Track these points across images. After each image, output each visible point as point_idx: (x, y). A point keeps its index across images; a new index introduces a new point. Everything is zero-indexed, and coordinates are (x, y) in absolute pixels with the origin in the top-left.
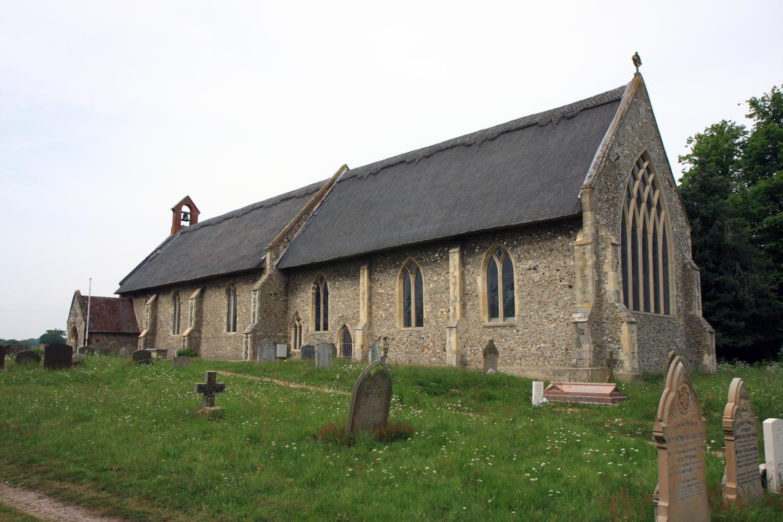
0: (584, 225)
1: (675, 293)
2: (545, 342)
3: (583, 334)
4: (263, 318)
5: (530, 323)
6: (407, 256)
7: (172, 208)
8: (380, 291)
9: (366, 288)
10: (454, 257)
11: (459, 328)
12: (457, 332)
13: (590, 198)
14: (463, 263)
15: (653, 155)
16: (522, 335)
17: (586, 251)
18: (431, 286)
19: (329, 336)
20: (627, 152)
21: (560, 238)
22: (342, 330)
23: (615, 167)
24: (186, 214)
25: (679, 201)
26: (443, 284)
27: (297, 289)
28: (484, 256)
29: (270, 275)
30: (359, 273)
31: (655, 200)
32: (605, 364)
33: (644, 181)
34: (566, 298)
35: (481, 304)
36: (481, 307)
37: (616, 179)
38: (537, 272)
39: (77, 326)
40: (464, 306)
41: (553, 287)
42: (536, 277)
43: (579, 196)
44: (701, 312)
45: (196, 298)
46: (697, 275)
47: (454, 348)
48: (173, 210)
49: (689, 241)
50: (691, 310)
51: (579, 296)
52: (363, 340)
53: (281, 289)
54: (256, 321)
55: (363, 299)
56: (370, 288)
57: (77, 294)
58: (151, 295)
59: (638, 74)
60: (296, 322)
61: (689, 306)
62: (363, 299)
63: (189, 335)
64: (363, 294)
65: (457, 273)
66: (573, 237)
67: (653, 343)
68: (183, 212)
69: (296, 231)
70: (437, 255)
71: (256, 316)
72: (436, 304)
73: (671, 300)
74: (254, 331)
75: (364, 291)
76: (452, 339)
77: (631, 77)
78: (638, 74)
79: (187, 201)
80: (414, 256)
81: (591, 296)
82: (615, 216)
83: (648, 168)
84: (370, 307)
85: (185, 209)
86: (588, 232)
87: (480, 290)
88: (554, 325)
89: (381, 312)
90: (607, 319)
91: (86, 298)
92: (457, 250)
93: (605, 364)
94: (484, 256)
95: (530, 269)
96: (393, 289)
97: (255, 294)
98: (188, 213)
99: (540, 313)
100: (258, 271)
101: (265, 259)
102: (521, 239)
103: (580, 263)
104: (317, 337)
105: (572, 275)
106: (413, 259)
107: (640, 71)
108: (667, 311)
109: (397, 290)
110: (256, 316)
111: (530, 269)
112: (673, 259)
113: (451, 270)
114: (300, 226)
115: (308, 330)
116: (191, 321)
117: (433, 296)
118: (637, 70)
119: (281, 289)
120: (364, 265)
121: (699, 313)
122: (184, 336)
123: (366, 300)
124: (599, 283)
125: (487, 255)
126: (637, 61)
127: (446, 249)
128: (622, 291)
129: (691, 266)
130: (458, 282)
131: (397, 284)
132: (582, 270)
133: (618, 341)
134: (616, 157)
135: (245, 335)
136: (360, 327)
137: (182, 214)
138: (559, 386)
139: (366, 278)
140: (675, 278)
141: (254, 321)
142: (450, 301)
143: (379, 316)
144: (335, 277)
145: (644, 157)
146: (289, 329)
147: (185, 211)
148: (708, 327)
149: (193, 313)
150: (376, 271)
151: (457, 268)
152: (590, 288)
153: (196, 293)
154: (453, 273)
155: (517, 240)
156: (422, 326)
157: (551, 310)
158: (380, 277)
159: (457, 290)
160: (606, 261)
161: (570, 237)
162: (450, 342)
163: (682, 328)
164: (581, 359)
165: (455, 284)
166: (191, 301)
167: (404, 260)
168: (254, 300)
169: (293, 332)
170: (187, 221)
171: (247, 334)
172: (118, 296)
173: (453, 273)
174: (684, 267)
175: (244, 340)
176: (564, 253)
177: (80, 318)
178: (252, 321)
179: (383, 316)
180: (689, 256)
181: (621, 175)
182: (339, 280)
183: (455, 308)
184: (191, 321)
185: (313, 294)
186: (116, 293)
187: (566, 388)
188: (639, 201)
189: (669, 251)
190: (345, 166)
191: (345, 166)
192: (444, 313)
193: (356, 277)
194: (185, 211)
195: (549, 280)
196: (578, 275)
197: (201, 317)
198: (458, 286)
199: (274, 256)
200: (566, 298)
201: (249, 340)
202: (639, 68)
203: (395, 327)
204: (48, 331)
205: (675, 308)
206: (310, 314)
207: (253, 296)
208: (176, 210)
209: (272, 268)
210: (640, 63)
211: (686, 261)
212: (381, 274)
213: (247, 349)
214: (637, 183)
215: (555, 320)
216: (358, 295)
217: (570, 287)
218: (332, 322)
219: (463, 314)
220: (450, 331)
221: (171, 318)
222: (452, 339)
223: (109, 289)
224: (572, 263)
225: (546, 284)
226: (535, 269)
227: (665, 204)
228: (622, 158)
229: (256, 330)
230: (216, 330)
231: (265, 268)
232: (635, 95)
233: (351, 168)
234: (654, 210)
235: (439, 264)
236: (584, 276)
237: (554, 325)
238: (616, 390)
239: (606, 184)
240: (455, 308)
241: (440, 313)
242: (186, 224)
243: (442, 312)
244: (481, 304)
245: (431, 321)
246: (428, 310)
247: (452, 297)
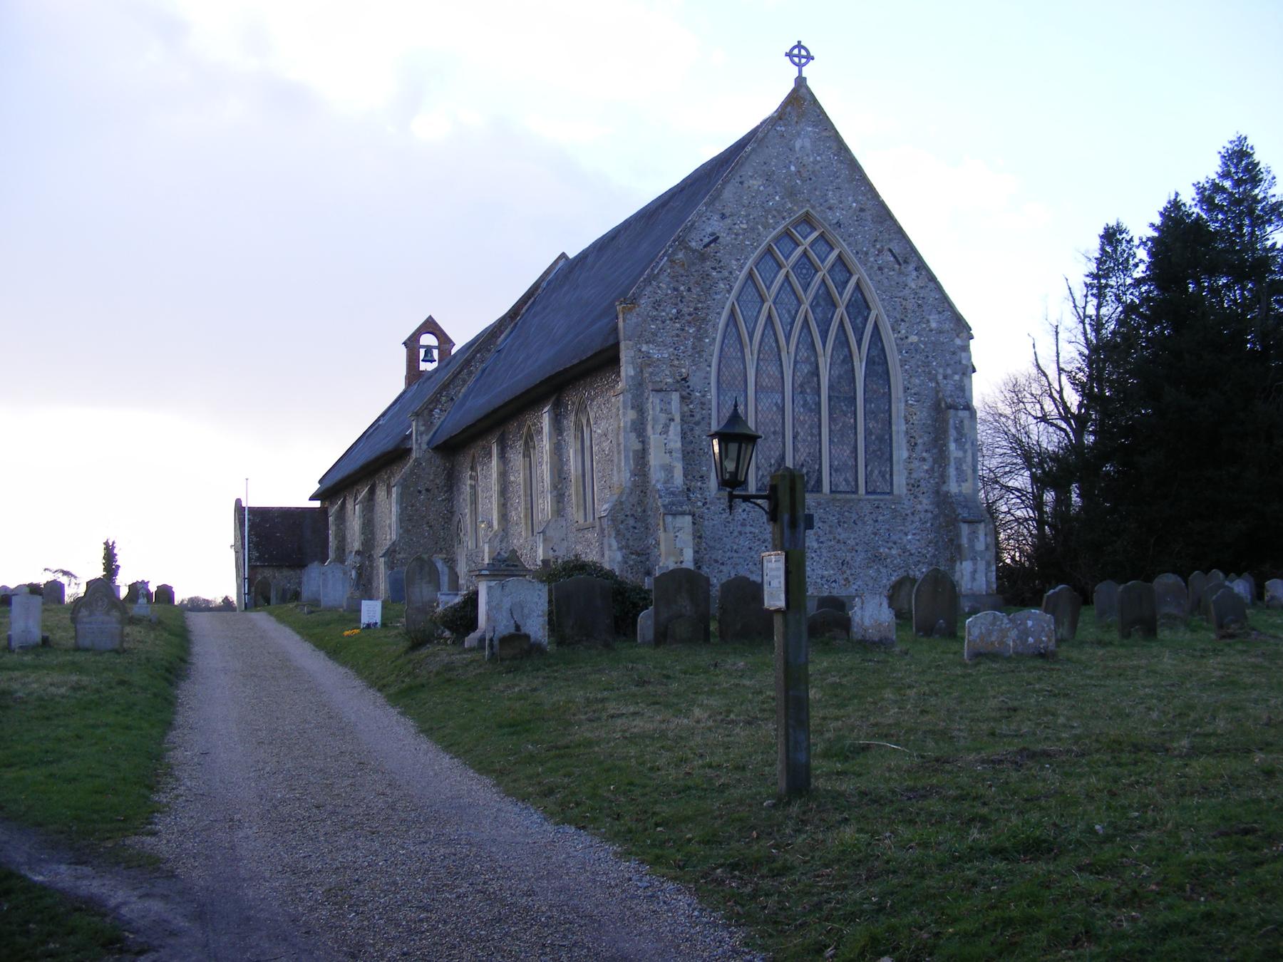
4: (407, 531)
11: (550, 533)
20: (744, 226)
24: (429, 350)
59: (801, 81)
68: (423, 347)
69: (464, 381)
78: (801, 81)
85: (428, 340)
98: (435, 347)
114: (470, 373)
126: (800, 55)
137: (422, 352)
172: (317, 504)
186: (312, 499)
190: (563, 255)
191: (563, 255)
197: (372, 533)
199: (422, 428)
202: (806, 72)
204: (118, 567)
208: (412, 344)
233: (571, 255)
239: (676, 289)
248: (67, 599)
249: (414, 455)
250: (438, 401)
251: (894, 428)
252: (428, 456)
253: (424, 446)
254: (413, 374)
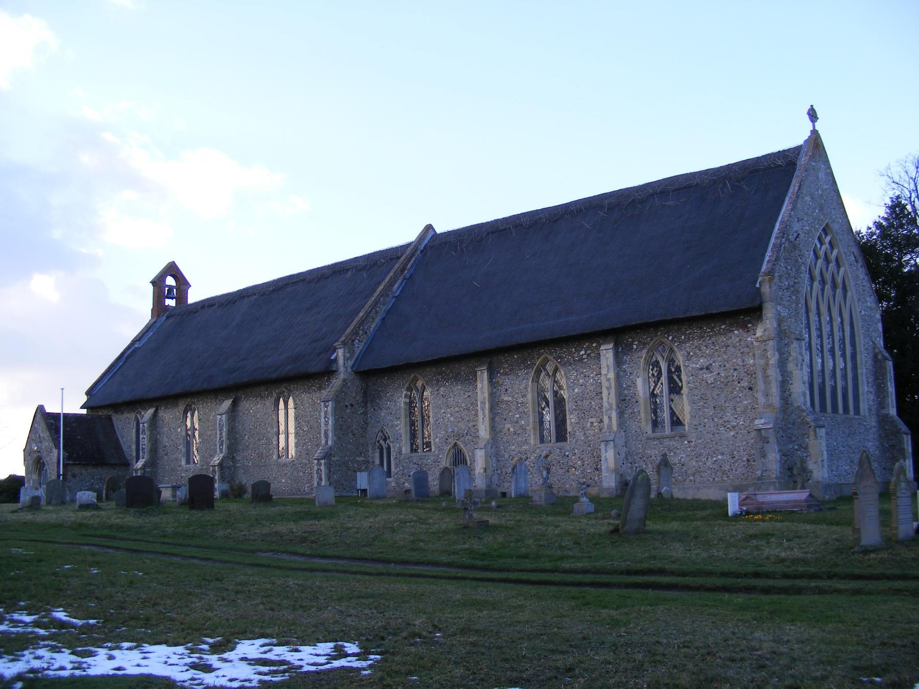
0: (764, 318)
1: (866, 389)
2: (723, 454)
3: (768, 442)
4: (339, 438)
5: (704, 432)
6: (542, 354)
7: (151, 280)
8: (506, 399)
9: (486, 395)
10: (607, 352)
11: (617, 441)
12: (615, 447)
13: (770, 287)
14: (618, 362)
15: (835, 227)
16: (696, 446)
17: (768, 348)
18: (576, 390)
19: (432, 458)
21: (736, 332)
22: (453, 450)
23: (795, 247)
24: (171, 288)
25: (866, 278)
26: (592, 388)
27: (380, 398)
28: (644, 353)
29: (344, 380)
30: (476, 376)
31: (839, 280)
32: (794, 473)
33: (827, 260)
34: (745, 402)
35: (642, 411)
36: (642, 415)
37: (797, 261)
38: (711, 372)
39: (44, 454)
40: (621, 414)
41: (730, 389)
42: (709, 377)
43: (758, 285)
44: (895, 410)
45: (226, 413)
46: (890, 364)
47: (612, 464)
48: (153, 283)
49: (880, 325)
50: (883, 408)
51: (761, 399)
52: (487, 462)
53: (358, 398)
54: (330, 443)
55: (483, 409)
56: (492, 395)
57: (40, 409)
58: (146, 409)
59: (814, 132)
60: (382, 442)
61: (882, 404)
62: (483, 409)
63: (221, 465)
64: (483, 403)
65: (611, 375)
66: (752, 332)
67: (842, 448)
69: (373, 319)
70: (582, 352)
71: (330, 435)
72: (584, 414)
73: (861, 398)
74: (327, 456)
75: (484, 398)
76: (609, 456)
77: (806, 135)
78: (814, 132)
79: (172, 269)
80: (551, 354)
81: (776, 400)
82: (797, 304)
83: (830, 243)
84: (492, 420)
85: (170, 281)
86: (769, 326)
87: (641, 394)
88: (732, 433)
89: (508, 426)
90: (793, 424)
91: (56, 416)
92: (611, 346)
93: (794, 473)
94: (644, 353)
95: (701, 369)
96: (524, 396)
97: (327, 407)
99: (716, 420)
100: (328, 372)
101: (336, 358)
102: (690, 333)
103: (762, 362)
104: (415, 461)
105: (751, 374)
106: (550, 357)
107: (817, 128)
108: (857, 410)
109: (529, 396)
110: (330, 435)
111: (701, 369)
112: (862, 349)
113: (604, 371)
114: (377, 312)
115: (400, 452)
116: (221, 445)
117: (579, 403)
118: (814, 126)
119: (358, 398)
120: (482, 364)
121: (893, 411)
122: (214, 466)
123: (487, 411)
124: (784, 384)
125: (648, 352)
126: (813, 115)
127: (594, 345)
128: (808, 392)
129: (883, 355)
130: (613, 386)
131: (529, 389)
132: (764, 370)
133: (806, 448)
134: (795, 235)
135: (316, 462)
136: (482, 445)
138: (753, 497)
139: (486, 382)
140: (864, 371)
141: (327, 442)
142: (604, 410)
143: (506, 430)
144: (438, 381)
145: (825, 231)
146: (370, 452)
147: (169, 283)
148: (903, 427)
149: (224, 434)
150: (498, 372)
151: (612, 370)
152: (775, 390)
153: (227, 404)
154: (606, 375)
155: (685, 334)
156: (565, 440)
157: (729, 416)
158: (506, 381)
159: (613, 395)
160: (790, 359)
161: (748, 331)
162: (606, 459)
163: (874, 430)
164: (766, 471)
165: (608, 388)
166: (219, 417)
167: (538, 358)
168: (326, 413)
169: (377, 455)
170: (172, 298)
171: (318, 460)
172: (84, 411)
173: (606, 375)
174: (875, 356)
175: (316, 468)
176: (742, 350)
177: (48, 443)
178: (323, 442)
179: (511, 430)
180: (880, 342)
181: (801, 256)
182: (444, 385)
183: (610, 418)
184: (221, 445)
185: (405, 403)
187: (760, 498)
188: (823, 282)
189: (857, 339)
191: (429, 228)
192: (595, 424)
193: (471, 379)
194: (169, 283)
195: (726, 381)
196: (760, 375)
198: (613, 391)
199: (348, 355)
200: (745, 402)
201: (323, 468)
203: (528, 444)
205: (866, 407)
206: (402, 431)
207: (323, 409)
208: (158, 283)
209: (346, 371)
210: (817, 118)
211: (876, 350)
212: (506, 377)
213: (321, 479)
214: (820, 261)
215: (734, 427)
216: (474, 404)
217: (750, 389)
218: (437, 440)
219: (621, 424)
220: (606, 446)
221: (182, 441)
222: (609, 456)
223: (73, 404)
224: (752, 362)
225: (722, 386)
226: (707, 368)
227: (850, 284)
228: (802, 236)
229: (331, 455)
230: (260, 456)
231: (336, 371)
232: (812, 157)
234: (839, 291)
235: (585, 363)
236: (766, 377)
237: (732, 433)
238: (811, 495)
240: (610, 418)
241: (589, 425)
242: (171, 303)
243: (592, 423)
244: (642, 411)
245: (577, 433)
246: (573, 421)
247: (605, 404)
248: (730, 513)
249: (342, 376)
250: (357, 334)
251: (859, 371)
252: (351, 378)
253: (349, 370)
254: (158, 307)
